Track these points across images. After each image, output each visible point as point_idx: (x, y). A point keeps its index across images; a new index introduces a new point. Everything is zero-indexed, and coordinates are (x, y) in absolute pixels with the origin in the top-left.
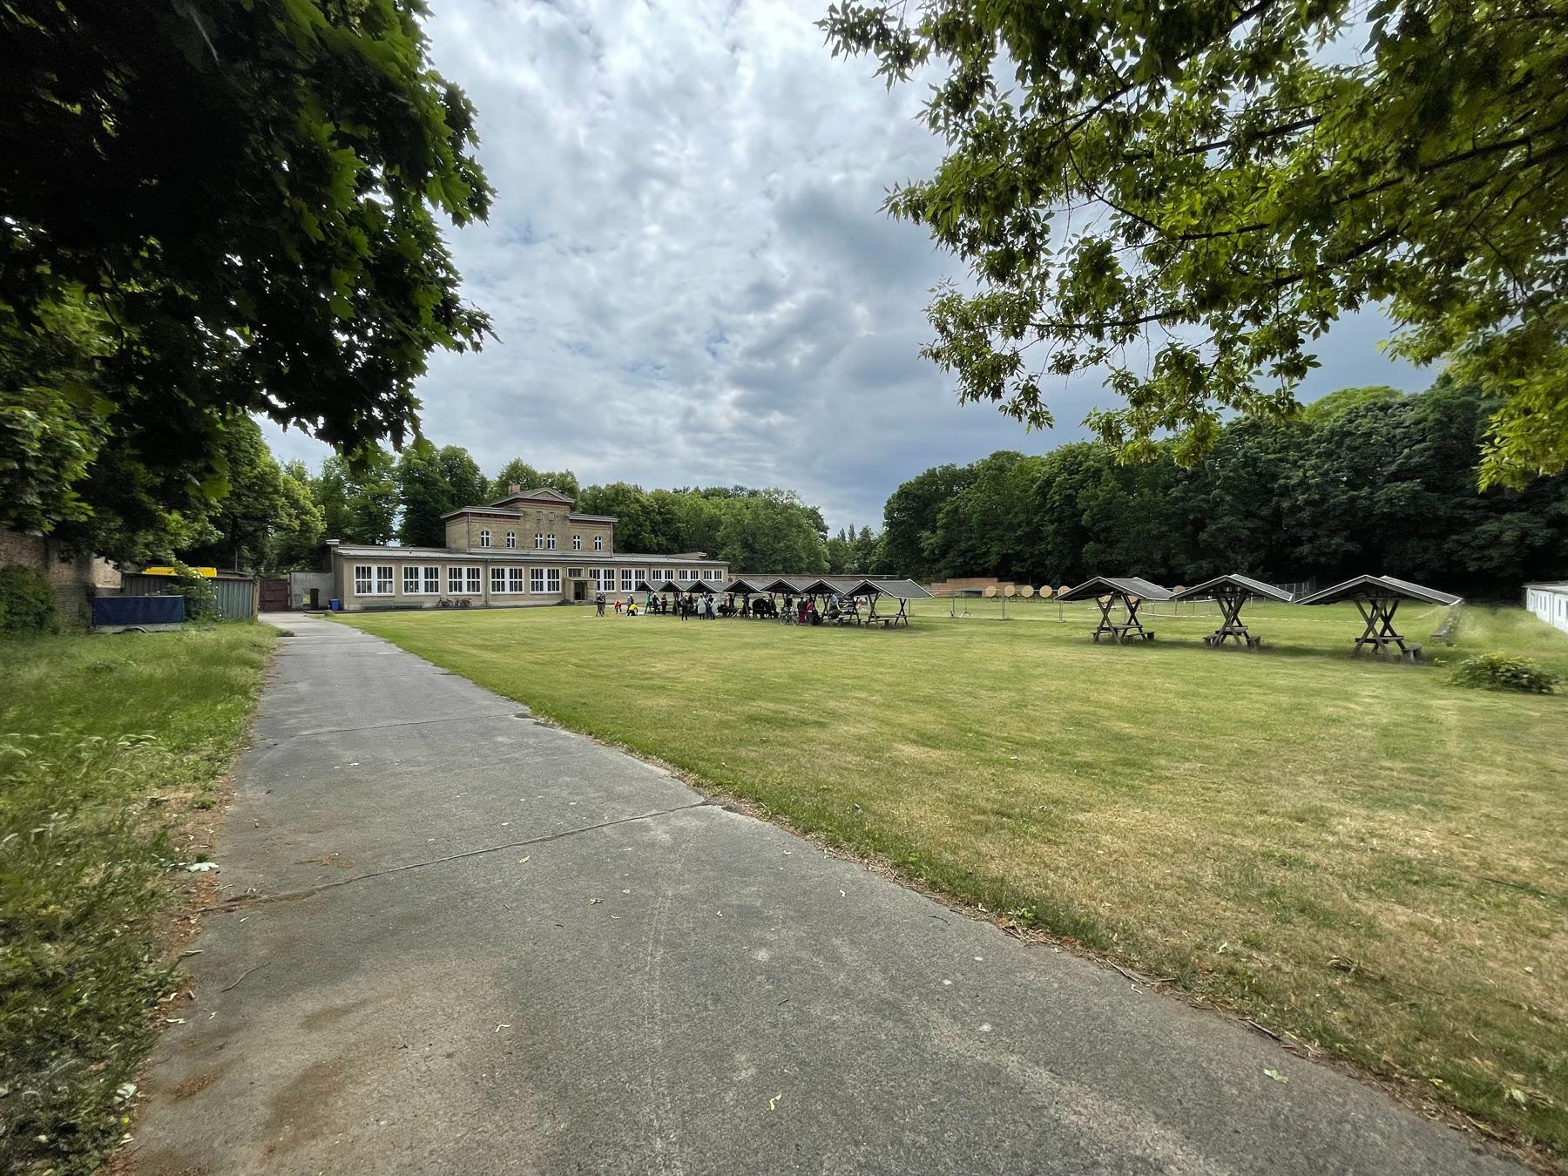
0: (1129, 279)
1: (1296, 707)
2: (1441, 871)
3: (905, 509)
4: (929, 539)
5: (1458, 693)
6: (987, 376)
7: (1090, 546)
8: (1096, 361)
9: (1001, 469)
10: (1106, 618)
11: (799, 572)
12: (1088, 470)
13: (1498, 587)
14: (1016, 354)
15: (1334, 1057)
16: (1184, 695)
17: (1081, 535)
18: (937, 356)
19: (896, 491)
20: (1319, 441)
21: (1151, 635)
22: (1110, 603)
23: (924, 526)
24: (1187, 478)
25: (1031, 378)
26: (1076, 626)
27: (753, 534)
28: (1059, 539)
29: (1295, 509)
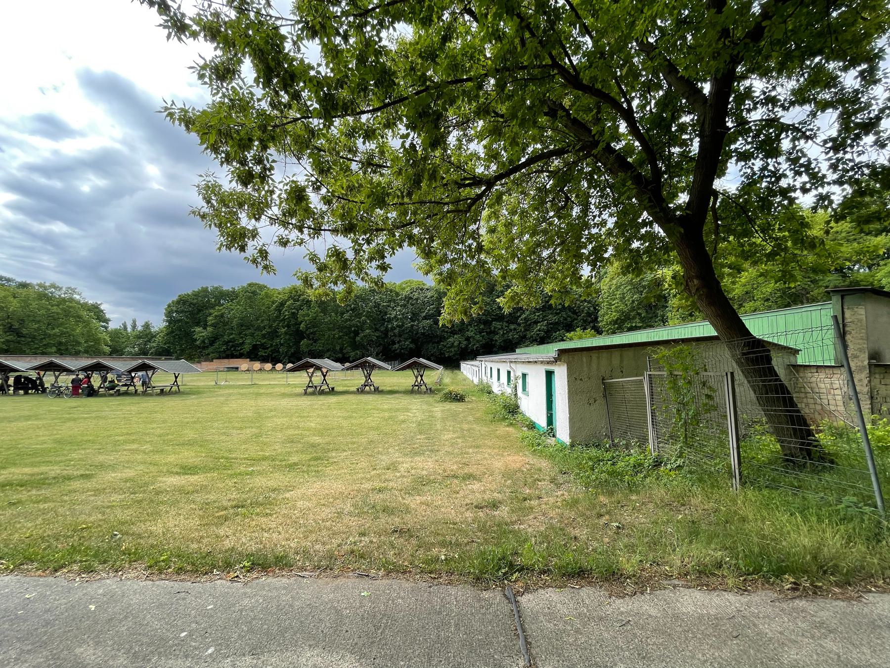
0: (316, 208)
1: (390, 418)
2: (432, 478)
3: (182, 312)
4: (200, 333)
5: (441, 405)
6: (238, 238)
7: (304, 342)
8: (300, 244)
9: (254, 293)
10: (311, 381)
11: (77, 354)
12: (303, 300)
13: (452, 363)
14: (256, 229)
15: (388, 573)
16: (345, 418)
17: (299, 335)
18: (203, 217)
19: (175, 298)
20: (401, 299)
21: (333, 389)
22: (313, 373)
23: (198, 324)
24: (351, 310)
25: (264, 245)
26: (295, 386)
27: (22, 321)
28: (287, 337)
29: (393, 329)
